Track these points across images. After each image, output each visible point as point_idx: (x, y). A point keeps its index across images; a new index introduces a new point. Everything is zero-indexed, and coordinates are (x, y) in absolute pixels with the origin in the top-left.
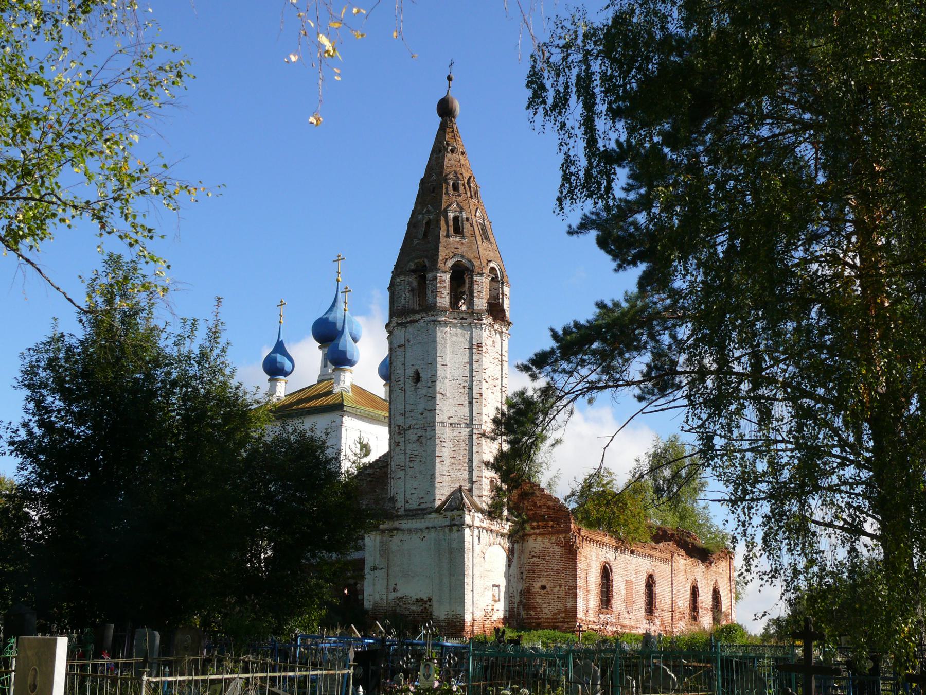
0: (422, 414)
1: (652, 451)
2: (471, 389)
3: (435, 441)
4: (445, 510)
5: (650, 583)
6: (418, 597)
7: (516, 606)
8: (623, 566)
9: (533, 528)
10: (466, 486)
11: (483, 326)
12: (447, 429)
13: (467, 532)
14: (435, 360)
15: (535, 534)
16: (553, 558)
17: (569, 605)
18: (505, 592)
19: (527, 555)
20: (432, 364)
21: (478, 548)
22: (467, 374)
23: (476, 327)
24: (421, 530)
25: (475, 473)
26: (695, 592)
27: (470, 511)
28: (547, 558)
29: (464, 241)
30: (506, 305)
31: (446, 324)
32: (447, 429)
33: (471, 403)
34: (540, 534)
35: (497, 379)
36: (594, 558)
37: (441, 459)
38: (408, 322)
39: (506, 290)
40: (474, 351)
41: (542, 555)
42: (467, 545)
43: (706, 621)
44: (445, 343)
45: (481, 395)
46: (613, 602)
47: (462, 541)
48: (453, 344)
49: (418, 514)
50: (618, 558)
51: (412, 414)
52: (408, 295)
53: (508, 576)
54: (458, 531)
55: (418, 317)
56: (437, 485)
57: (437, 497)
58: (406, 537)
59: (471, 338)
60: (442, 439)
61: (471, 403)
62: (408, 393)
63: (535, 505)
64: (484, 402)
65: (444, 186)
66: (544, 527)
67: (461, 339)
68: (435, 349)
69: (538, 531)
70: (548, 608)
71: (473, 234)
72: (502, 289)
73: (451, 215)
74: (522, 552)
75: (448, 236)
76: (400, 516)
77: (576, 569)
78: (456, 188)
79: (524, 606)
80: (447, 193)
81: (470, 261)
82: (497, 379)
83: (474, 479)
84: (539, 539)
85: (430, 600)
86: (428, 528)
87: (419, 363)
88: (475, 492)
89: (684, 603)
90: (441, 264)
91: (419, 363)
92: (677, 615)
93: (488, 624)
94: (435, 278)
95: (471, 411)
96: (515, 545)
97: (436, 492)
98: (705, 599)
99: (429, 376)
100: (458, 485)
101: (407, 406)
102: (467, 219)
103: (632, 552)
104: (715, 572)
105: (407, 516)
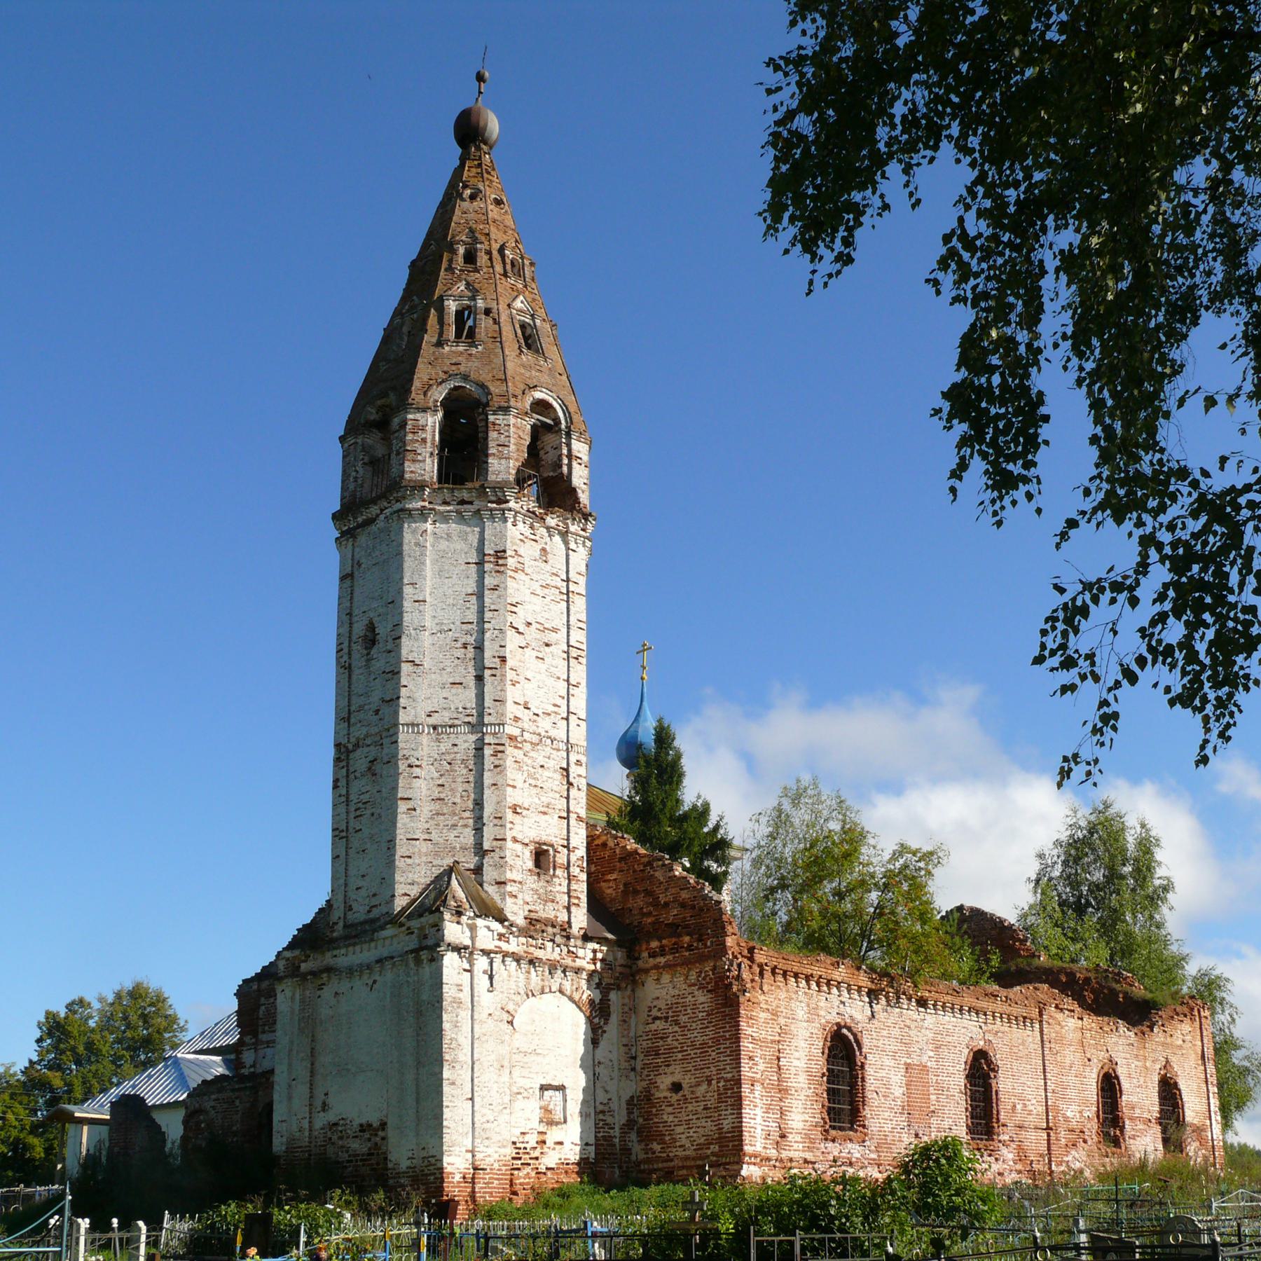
0: (377, 712)
1: (1064, 836)
2: (479, 648)
3: (396, 765)
4: (408, 917)
5: (981, 1071)
6: (364, 1121)
7: (617, 1132)
8: (896, 1032)
9: (653, 955)
10: (470, 861)
11: (509, 515)
12: (425, 739)
13: (451, 964)
14: (400, 592)
15: (656, 967)
16: (693, 1019)
17: (727, 1124)
18: (584, 1102)
19: (643, 1016)
20: (395, 603)
21: (486, 1001)
22: (472, 616)
23: (492, 517)
24: (369, 967)
25: (489, 833)
26: (1109, 1086)
27: (459, 914)
28: (683, 1019)
29: (474, 351)
30: (579, 477)
31: (423, 515)
32: (425, 739)
33: (479, 679)
34: (669, 967)
35: (555, 630)
36: (801, 1013)
37: (410, 804)
38: (359, 526)
39: (580, 448)
40: (488, 567)
41: (671, 1015)
42: (449, 992)
43: (1145, 1143)
44: (423, 554)
45: (503, 659)
46: (867, 1112)
47: (438, 984)
48: (442, 556)
49: (365, 932)
50: (881, 1015)
51: (362, 715)
52: (361, 471)
53: (591, 1065)
54: (432, 960)
55: (374, 510)
56: (400, 863)
57: (400, 889)
58: (344, 986)
59: (482, 541)
60: (413, 761)
61: (479, 679)
62: (356, 672)
63: (656, 903)
64: (510, 675)
65: (446, 256)
66: (676, 949)
67: (459, 545)
68: (400, 569)
69: (662, 960)
70: (686, 1133)
71: (498, 338)
72: (569, 445)
73: (452, 306)
74: (634, 1009)
75: (439, 344)
76: (337, 939)
77: (738, 1040)
78: (470, 258)
79: (639, 1133)
80: (450, 269)
81: (482, 386)
82: (555, 630)
83: (486, 846)
84: (666, 978)
85: (383, 1125)
86: (379, 961)
87: (375, 605)
88: (489, 874)
89: (1080, 1106)
90: (416, 396)
91: (375, 605)
92: (1063, 1137)
93: (524, 1177)
94: (403, 424)
95: (480, 696)
96: (613, 996)
97: (398, 877)
98: (1140, 1097)
99: (390, 627)
100: (448, 861)
101: (354, 700)
102: (488, 312)
103: (922, 1003)
104: (1163, 1044)
105: (346, 938)
